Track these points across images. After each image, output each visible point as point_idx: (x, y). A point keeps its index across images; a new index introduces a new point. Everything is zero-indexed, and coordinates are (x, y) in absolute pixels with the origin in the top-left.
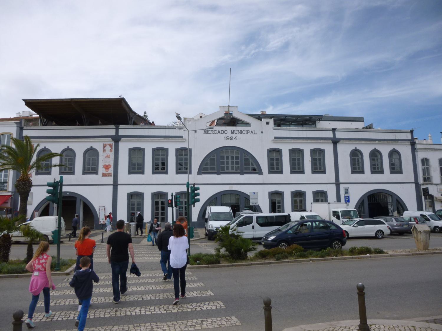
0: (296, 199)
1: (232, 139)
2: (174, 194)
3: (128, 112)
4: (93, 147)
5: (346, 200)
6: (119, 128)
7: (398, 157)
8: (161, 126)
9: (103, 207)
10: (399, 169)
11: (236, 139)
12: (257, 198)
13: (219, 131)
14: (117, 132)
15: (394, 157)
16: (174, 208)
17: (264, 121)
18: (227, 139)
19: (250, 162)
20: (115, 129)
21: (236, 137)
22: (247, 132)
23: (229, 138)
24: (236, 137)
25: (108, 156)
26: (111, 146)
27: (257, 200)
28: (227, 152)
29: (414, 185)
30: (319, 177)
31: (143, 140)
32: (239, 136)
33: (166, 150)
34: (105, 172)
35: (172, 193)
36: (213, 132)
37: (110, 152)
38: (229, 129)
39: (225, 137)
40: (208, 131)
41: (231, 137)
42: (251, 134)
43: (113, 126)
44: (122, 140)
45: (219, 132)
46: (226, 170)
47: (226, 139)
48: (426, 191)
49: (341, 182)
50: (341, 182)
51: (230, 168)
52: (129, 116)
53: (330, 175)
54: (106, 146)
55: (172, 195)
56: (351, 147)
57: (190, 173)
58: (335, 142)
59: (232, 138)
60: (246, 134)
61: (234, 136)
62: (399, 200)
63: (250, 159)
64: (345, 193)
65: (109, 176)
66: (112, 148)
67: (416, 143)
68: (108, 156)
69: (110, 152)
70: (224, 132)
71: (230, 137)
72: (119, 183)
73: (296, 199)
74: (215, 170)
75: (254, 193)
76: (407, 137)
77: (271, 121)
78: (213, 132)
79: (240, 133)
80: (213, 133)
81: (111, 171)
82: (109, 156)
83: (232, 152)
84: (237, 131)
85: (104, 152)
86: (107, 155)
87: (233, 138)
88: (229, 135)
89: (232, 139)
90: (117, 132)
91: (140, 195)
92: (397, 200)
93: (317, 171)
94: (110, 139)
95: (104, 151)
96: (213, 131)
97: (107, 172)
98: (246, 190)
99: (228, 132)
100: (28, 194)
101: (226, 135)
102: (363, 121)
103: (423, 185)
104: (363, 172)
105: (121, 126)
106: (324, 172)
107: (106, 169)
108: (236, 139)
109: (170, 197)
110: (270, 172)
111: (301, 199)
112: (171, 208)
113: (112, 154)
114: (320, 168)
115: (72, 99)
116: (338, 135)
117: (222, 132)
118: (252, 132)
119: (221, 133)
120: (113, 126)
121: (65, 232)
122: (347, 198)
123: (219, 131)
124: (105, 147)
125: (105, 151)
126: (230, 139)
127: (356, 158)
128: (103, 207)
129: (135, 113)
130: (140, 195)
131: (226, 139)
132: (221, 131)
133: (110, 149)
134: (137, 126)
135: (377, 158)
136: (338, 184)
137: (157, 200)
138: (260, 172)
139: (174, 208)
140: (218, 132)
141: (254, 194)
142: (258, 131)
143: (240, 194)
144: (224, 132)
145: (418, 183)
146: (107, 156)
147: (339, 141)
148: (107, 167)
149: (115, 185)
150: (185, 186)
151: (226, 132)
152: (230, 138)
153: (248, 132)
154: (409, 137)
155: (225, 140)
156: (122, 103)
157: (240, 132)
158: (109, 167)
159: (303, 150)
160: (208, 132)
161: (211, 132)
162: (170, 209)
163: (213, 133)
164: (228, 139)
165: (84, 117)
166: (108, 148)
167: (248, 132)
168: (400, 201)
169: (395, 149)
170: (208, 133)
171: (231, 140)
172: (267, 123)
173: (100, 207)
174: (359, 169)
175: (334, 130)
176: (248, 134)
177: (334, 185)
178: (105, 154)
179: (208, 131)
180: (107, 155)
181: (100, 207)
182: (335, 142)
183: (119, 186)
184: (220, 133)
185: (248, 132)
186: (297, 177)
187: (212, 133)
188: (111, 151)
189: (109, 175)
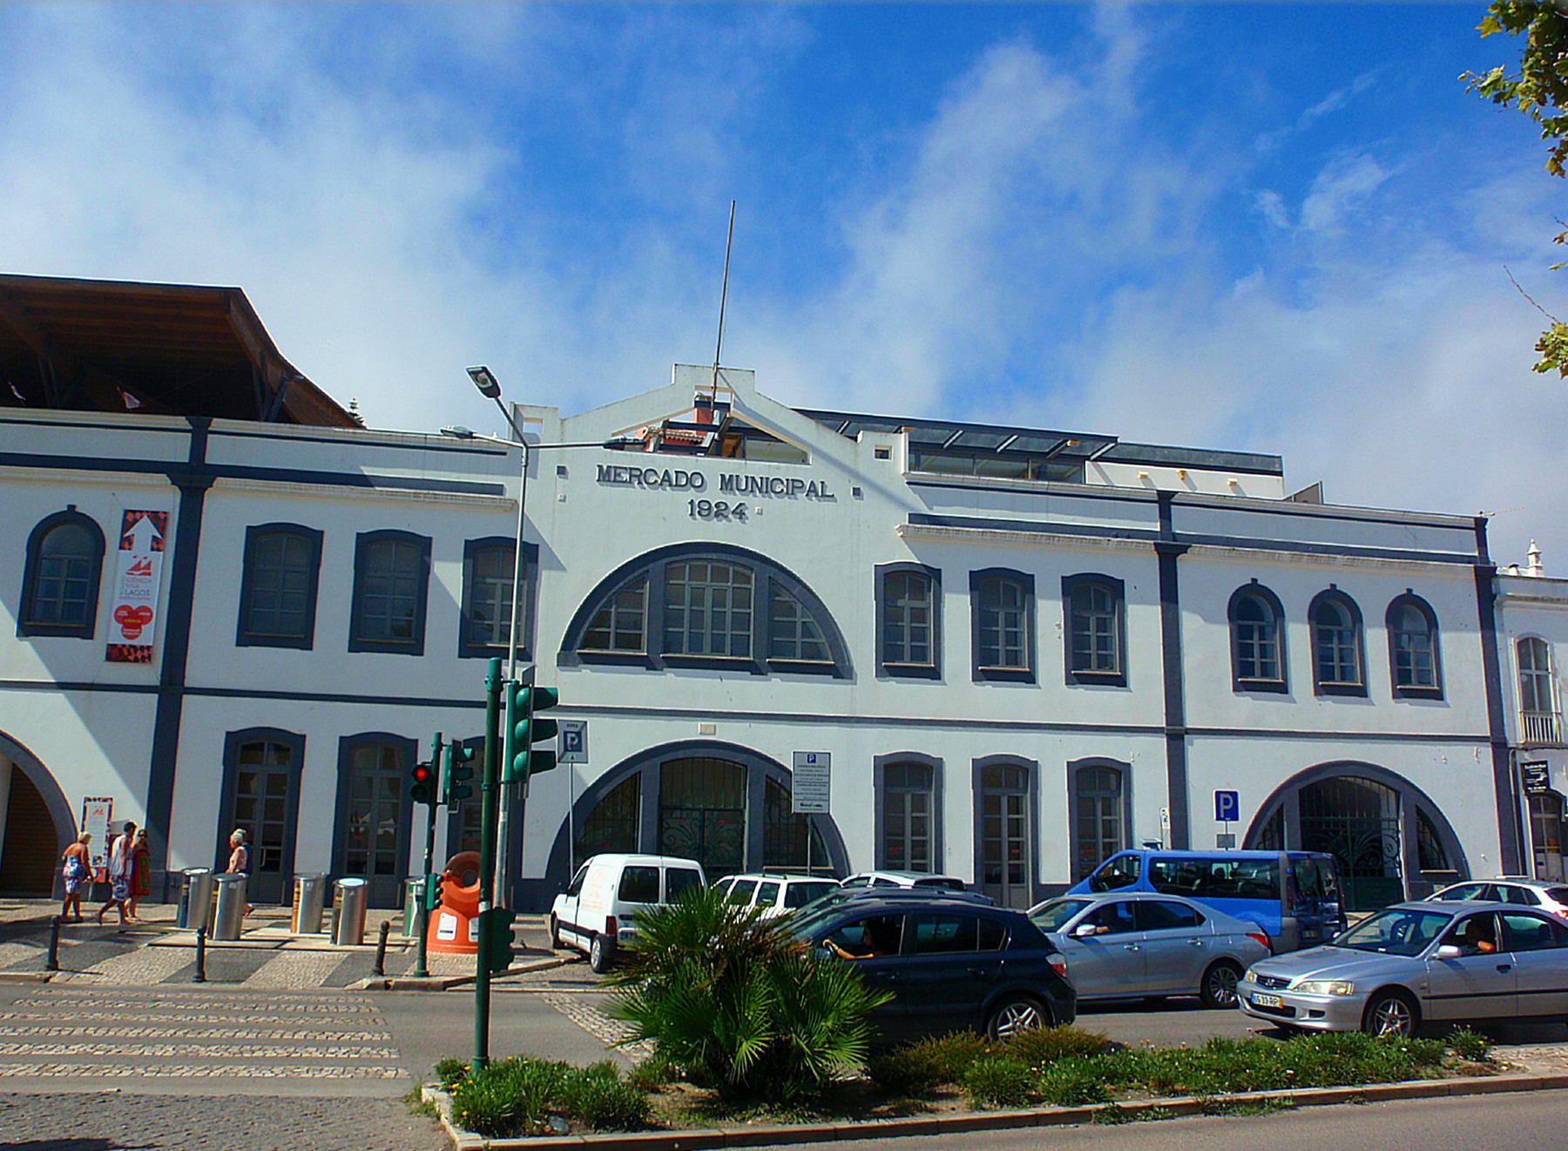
0: (994, 792)
2: (446, 741)
6: (210, 429)
7: (1424, 626)
9: (105, 800)
14: (198, 448)
16: (443, 812)
17: (868, 440)
19: (799, 620)
22: (794, 487)
25: (142, 569)
27: (824, 790)
28: (697, 574)
29: (1487, 752)
32: (754, 502)
33: (310, 541)
34: (120, 640)
35: (440, 735)
36: (638, 476)
37: (152, 549)
38: (714, 468)
40: (618, 471)
41: (717, 505)
43: (184, 418)
45: (669, 481)
48: (1538, 776)
49: (1190, 723)
50: (1190, 723)
51: (708, 598)
54: (136, 521)
55: (439, 746)
56: (1235, 573)
61: (733, 500)
65: (136, 660)
66: (162, 531)
68: (142, 569)
69: (152, 549)
70: (689, 480)
72: (188, 683)
73: (994, 792)
74: (639, 648)
75: (812, 758)
77: (900, 444)
78: (638, 476)
81: (152, 635)
82: (148, 566)
83: (720, 575)
84: (747, 477)
85: (121, 548)
88: (714, 494)
90: (198, 448)
92: (1419, 812)
94: (163, 478)
95: (126, 543)
96: (638, 473)
98: (779, 744)
101: (697, 497)
102: (1280, 474)
103: (1523, 749)
105: (217, 423)
106: (1120, 682)
107: (126, 626)
108: (740, 512)
109: (425, 755)
112: (426, 807)
116: (1183, 523)
118: (812, 489)
120: (181, 421)
125: (131, 544)
126: (713, 514)
128: (105, 800)
130: (289, 747)
133: (154, 538)
134: (295, 426)
136: (1176, 735)
138: (840, 670)
139: (443, 812)
140: (663, 480)
141: (814, 761)
142: (839, 486)
146: (137, 567)
147: (1184, 550)
148: (133, 619)
153: (793, 487)
157: (766, 487)
160: (615, 475)
162: (420, 810)
167: (796, 484)
170: (615, 481)
172: (883, 454)
173: (89, 800)
175: (1165, 500)
177: (1162, 742)
178: (126, 559)
181: (89, 800)
183: (187, 700)
185: (796, 484)
188: (157, 545)
189: (139, 654)
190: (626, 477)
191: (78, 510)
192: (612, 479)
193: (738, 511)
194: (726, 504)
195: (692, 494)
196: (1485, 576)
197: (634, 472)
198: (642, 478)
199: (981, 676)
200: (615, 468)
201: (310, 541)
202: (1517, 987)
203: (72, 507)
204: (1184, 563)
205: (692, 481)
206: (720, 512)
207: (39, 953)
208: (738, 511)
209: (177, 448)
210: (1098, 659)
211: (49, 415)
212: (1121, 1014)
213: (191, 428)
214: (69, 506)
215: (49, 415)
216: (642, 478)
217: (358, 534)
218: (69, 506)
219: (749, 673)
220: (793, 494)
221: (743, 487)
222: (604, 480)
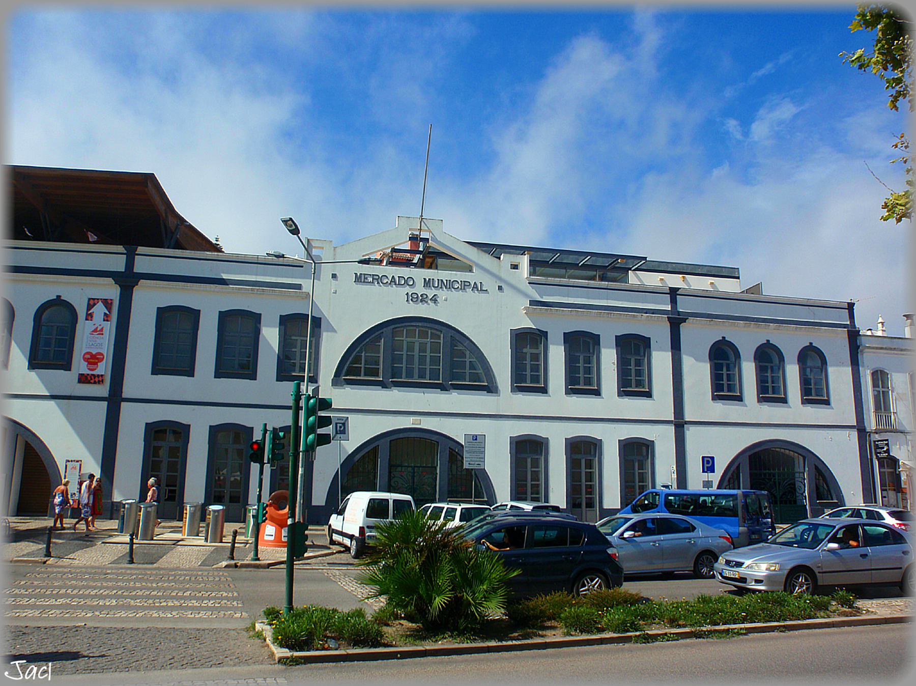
1: (426, 300)
2: (269, 428)
3: (164, 215)
4: (62, 298)
5: (706, 465)
6: (136, 253)
9: (77, 461)
12: (481, 452)
14: (130, 263)
15: (809, 363)
18: (411, 300)
19: (468, 360)
22: (465, 285)
23: (417, 297)
25: (98, 331)
26: (108, 303)
27: (482, 456)
28: (410, 334)
29: (854, 434)
32: (442, 294)
36: (377, 279)
37: (104, 320)
40: (366, 276)
41: (422, 295)
43: (122, 246)
45: (395, 282)
48: (883, 448)
52: (165, 227)
54: (95, 304)
61: (430, 293)
62: (820, 467)
63: (468, 353)
64: (337, 433)
65: (95, 383)
66: (109, 309)
68: (98, 331)
69: (104, 320)
70: (406, 282)
71: (419, 295)
72: (124, 396)
75: (475, 438)
76: (840, 319)
77: (524, 261)
78: (377, 279)
81: (104, 368)
82: (102, 330)
84: (438, 280)
85: (87, 319)
86: (96, 326)
88: (420, 289)
89: (426, 300)
90: (130, 263)
91: (181, 432)
92: (816, 468)
94: (110, 280)
95: (89, 316)
96: (377, 277)
97: (94, 373)
98: (456, 430)
101: (411, 291)
102: (738, 278)
103: (874, 433)
105: (141, 249)
107: (89, 363)
108: (434, 300)
109: (257, 436)
112: (258, 465)
113: (110, 328)
120: (120, 248)
122: (708, 462)
124: (93, 307)
125: (92, 317)
126: (419, 300)
127: (724, 362)
128: (77, 461)
129: (182, 220)
130: (181, 432)
133: (105, 314)
134: (184, 251)
135: (772, 365)
136: (680, 425)
138: (491, 388)
139: (267, 468)
140: (391, 281)
141: (476, 439)
142: (490, 284)
143: (804, 454)
144: (406, 282)
145: (865, 430)
146: (95, 330)
147: (684, 320)
148: (93, 359)
149: (115, 400)
153: (465, 285)
156: (147, 186)
157: (442, 284)
158: (98, 358)
159: (599, 336)
162: (255, 467)
166: (99, 310)
168: (823, 471)
170: (364, 282)
172: (515, 267)
173: (69, 461)
175: (674, 293)
177: (672, 428)
180: (97, 328)
181: (69, 461)
188: (107, 318)
190: (370, 279)
192: (363, 281)
193: (434, 298)
194: (426, 295)
197: (375, 277)
198: (379, 280)
199: (570, 391)
208: (434, 298)
213: (125, 252)
214: (57, 296)
215: (87, 247)
216: (379, 280)
218: (57, 296)
221: (436, 285)
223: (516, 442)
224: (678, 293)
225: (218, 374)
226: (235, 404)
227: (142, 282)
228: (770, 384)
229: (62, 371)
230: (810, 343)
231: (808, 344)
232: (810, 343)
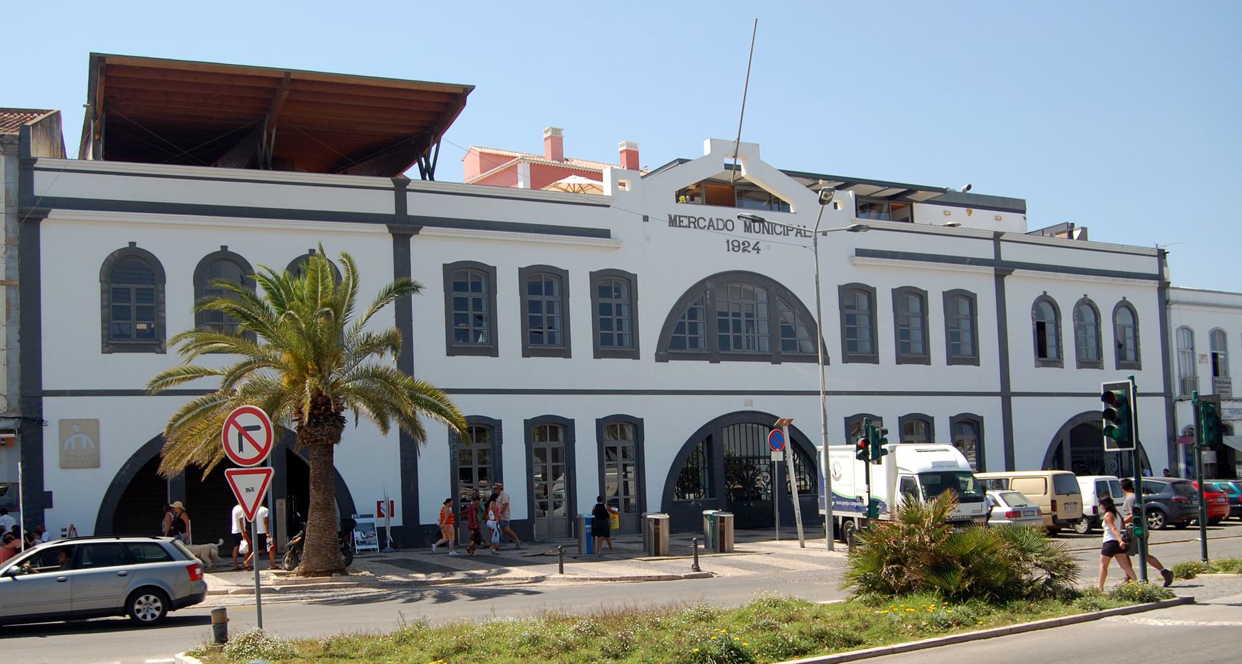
4: (137, 246)
8: (1129, 246)
10: (867, 347)
11: (758, 250)
13: (711, 220)
14: (401, 203)
18: (733, 249)
20: (393, 192)
21: (758, 243)
23: (739, 246)
24: (758, 243)
30: (963, 376)
31: (529, 240)
32: (764, 238)
33: (561, 277)
39: (728, 242)
40: (681, 219)
41: (743, 244)
42: (796, 235)
44: (424, 233)
45: (713, 226)
46: (690, 347)
47: (731, 247)
53: (985, 374)
57: (826, 362)
58: (1002, 269)
59: (747, 245)
60: (784, 235)
61: (752, 238)
67: (1171, 286)
70: (725, 225)
72: (45, 387)
79: (768, 233)
80: (695, 227)
87: (749, 245)
89: (749, 249)
93: (684, 351)
94: (383, 228)
99: (732, 219)
100: (852, 416)
104: (566, 353)
110: (846, 359)
111: (482, 446)
114: (552, 340)
115: (288, 72)
116: (1009, 253)
117: (721, 226)
118: (799, 232)
119: (718, 229)
121: (813, 524)
123: (711, 220)
126: (741, 249)
131: (731, 247)
132: (717, 220)
136: (1006, 395)
137: (542, 445)
140: (709, 226)
144: (725, 225)
150: (1160, 398)
151: (730, 225)
152: (742, 247)
153: (788, 230)
154: (1151, 267)
155: (729, 250)
160: (680, 221)
161: (690, 222)
163: (695, 227)
164: (736, 249)
165: (269, 135)
169: (1048, 294)
170: (680, 226)
171: (744, 251)
174: (621, 343)
175: (997, 237)
176: (788, 235)
179: (681, 219)
182: (1002, 269)
184: (714, 229)
186: (547, 370)
187: (692, 225)
190: (685, 222)
191: (1127, 300)
192: (716, 228)
193: (756, 248)
194: (748, 243)
195: (725, 235)
196: (1164, 286)
197: (692, 220)
198: (696, 224)
199: (900, 360)
200: (680, 217)
201: (561, 277)
202: (1188, 533)
203: (224, 248)
204: (1008, 281)
205: (726, 225)
206: (743, 247)
207: (820, 568)
208: (756, 248)
209: (384, 203)
210: (474, 333)
211: (337, 179)
212: (16, 639)
213: (393, 186)
214: (130, 243)
215: (337, 179)
216: (696, 224)
217: (943, 292)
218: (130, 243)
219: (770, 363)
220: (788, 235)
221: (758, 231)
222: (673, 226)
223: (901, 420)
224: (1001, 238)
225: (598, 354)
226: (648, 394)
227: (425, 230)
228: (545, 330)
229: (973, 366)
230: (1085, 295)
231: (219, 249)
232: (1085, 295)
